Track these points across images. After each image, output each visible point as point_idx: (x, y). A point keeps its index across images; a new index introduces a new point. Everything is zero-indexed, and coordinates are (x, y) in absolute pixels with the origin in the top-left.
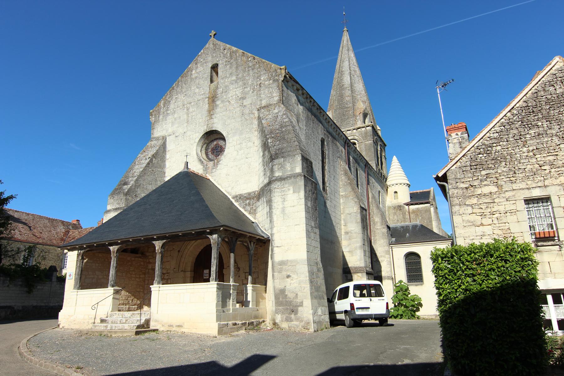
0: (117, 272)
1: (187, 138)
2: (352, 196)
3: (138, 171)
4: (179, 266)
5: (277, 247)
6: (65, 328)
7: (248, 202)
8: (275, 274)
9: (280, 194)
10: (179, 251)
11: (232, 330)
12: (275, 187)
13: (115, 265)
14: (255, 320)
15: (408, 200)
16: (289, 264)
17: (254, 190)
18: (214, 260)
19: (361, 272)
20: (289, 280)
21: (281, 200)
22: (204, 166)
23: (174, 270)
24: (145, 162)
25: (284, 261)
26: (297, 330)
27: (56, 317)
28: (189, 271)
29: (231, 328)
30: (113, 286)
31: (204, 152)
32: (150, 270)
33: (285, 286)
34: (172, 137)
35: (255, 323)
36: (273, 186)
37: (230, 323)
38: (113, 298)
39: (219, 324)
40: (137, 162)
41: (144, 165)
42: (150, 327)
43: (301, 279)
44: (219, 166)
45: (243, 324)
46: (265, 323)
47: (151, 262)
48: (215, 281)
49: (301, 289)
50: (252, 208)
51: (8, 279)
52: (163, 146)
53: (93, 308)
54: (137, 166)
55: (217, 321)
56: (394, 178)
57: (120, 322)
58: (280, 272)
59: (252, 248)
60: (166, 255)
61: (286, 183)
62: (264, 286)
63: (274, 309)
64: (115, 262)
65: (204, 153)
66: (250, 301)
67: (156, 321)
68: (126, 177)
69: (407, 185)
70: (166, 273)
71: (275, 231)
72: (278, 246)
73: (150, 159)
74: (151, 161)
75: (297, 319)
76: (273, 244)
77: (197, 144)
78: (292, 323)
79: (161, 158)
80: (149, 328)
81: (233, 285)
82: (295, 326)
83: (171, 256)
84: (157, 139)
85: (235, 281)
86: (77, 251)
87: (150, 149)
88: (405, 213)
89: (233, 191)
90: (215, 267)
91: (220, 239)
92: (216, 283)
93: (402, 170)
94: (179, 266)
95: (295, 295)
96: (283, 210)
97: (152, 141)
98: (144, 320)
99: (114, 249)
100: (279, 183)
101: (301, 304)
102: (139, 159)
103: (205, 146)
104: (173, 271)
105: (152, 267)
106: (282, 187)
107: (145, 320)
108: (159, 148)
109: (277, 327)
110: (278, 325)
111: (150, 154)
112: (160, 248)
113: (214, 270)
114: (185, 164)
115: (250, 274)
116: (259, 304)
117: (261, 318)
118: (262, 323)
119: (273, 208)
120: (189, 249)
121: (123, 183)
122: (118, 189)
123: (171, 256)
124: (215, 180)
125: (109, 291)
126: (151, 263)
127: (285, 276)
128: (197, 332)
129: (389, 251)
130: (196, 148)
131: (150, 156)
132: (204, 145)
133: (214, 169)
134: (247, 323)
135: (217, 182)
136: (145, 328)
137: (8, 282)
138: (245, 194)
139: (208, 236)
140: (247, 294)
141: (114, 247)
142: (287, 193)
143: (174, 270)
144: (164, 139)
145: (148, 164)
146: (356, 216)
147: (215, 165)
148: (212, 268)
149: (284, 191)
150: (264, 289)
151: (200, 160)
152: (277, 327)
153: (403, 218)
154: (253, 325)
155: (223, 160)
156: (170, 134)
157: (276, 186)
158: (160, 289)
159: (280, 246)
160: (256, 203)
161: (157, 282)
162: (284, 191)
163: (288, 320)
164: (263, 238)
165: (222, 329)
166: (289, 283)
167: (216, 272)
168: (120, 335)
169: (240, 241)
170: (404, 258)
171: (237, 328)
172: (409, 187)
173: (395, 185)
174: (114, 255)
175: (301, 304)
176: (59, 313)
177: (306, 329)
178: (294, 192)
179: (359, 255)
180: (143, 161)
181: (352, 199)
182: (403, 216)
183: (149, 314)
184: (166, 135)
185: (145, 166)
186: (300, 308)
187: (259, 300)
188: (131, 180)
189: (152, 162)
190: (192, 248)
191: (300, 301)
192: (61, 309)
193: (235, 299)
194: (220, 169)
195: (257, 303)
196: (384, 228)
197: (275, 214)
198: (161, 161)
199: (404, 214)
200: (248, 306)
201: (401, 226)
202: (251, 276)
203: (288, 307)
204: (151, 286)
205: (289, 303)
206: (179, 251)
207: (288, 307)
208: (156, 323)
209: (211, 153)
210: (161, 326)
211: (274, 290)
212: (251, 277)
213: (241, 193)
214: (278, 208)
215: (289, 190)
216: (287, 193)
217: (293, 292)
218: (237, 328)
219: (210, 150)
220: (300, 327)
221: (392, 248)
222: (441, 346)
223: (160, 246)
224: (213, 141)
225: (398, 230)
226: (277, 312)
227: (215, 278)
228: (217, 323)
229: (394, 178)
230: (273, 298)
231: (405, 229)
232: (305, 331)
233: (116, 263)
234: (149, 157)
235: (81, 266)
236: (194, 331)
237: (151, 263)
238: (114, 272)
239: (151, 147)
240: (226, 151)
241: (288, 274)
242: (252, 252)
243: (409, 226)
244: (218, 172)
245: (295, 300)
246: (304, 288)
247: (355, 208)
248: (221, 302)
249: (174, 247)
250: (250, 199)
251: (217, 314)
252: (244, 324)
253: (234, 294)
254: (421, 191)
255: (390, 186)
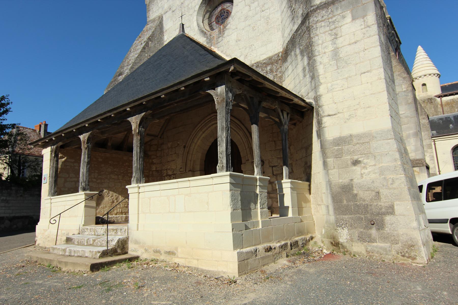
0: (90, 171)
1: (186, 9)
2: (399, 71)
3: (133, 58)
4: (186, 165)
5: (329, 116)
6: (40, 245)
7: (269, 68)
8: (328, 160)
9: (327, 29)
10: (184, 147)
11: (265, 261)
12: (317, 19)
13: (86, 160)
14: (300, 238)
15: (439, 92)
16: (355, 141)
17: (276, 52)
18: (222, 133)
19: (419, 165)
20: (357, 168)
21: (329, 38)
22: (207, 38)
23: (181, 170)
24: (140, 48)
25: (344, 137)
26: (388, 258)
27: (34, 230)
28: (199, 170)
29: (263, 258)
30: (84, 189)
31: (206, 22)
32: (154, 172)
33: (352, 180)
34: (169, 13)
35: (300, 243)
36: (313, 19)
37: (260, 247)
38: (86, 206)
39: (239, 254)
40: (132, 50)
41: (140, 50)
42: (129, 252)
43: (383, 164)
44: (226, 33)
45: (281, 247)
46: (314, 240)
47: (155, 162)
48: (227, 171)
49: (385, 184)
50: (277, 75)
51: (22, 188)
52: (159, 26)
53: (52, 221)
54: (132, 54)
55: (235, 247)
56: (424, 69)
57: (87, 242)
58: (338, 156)
59: (286, 122)
60: (170, 153)
61: (337, 9)
62: (308, 183)
63: (332, 218)
64: (86, 156)
65: (207, 24)
66: (288, 207)
67: (137, 242)
68: (121, 68)
69: (438, 75)
70: (172, 175)
71: (322, 90)
72: (331, 113)
73: (145, 43)
74: (147, 44)
75: (385, 238)
76: (321, 113)
77: (198, 13)
78: (375, 244)
79: (158, 40)
80: (126, 253)
81: (260, 178)
82: (382, 252)
83: (176, 153)
84: (154, 21)
85: (263, 173)
86: (50, 147)
87: (146, 33)
88: (437, 107)
89: (246, 60)
90: (224, 145)
91: (230, 95)
92: (228, 173)
93: (429, 60)
94: (186, 165)
95: (374, 193)
96: (336, 54)
97: (148, 24)
98: (116, 241)
99: (84, 137)
100: (323, 12)
101: (391, 210)
102: (134, 46)
103: (207, 16)
104: (180, 171)
105: (156, 169)
106: (330, 16)
107: (118, 242)
108: (155, 29)
109: (342, 250)
110: (343, 247)
111: (145, 38)
112: (138, 127)
113: (222, 151)
114: (180, 27)
115: (285, 164)
116: (302, 210)
117: (308, 233)
118: (309, 241)
119: (317, 54)
120: (196, 143)
121: (118, 74)
122: (113, 82)
123: (176, 153)
124: (222, 52)
125: (80, 196)
126: (155, 164)
127: (349, 162)
128: (200, 267)
129: (431, 145)
130: (197, 18)
131: (145, 39)
132: (206, 13)
133: (221, 38)
134: (289, 244)
135: (224, 54)
136: (119, 254)
137: (22, 192)
138: (263, 60)
139: (209, 91)
140: (282, 196)
141: (84, 135)
142: (340, 24)
143: (181, 170)
144: (161, 19)
145: (144, 48)
146: (407, 96)
147: (221, 33)
148: (219, 147)
149: (334, 22)
150: (308, 188)
151: (202, 32)
152: (342, 250)
153: (435, 111)
154: (298, 246)
155: (231, 23)
156: (167, 11)
157: (320, 18)
158: (141, 190)
159: (333, 113)
160: (281, 67)
161: (135, 179)
162: (334, 22)
163: (362, 238)
164: (303, 104)
165: (246, 261)
166: (359, 173)
167: (227, 155)
168: (71, 268)
169: (266, 110)
170: (451, 152)
171: (273, 256)
172: (439, 77)
173: (423, 76)
174: (84, 146)
175: (391, 210)
176: (37, 226)
177: (408, 257)
178: (354, 18)
179: (414, 144)
180: (139, 47)
181: (399, 75)
182: (435, 109)
183: (127, 230)
184: (163, 13)
185: (141, 52)
186: (388, 219)
187: (302, 205)
188: (126, 69)
189: (148, 46)
190: (199, 141)
191: (387, 204)
192: (38, 221)
193: (266, 204)
194: (228, 36)
195: (300, 210)
196: (424, 119)
197: (321, 63)
198: (158, 43)
199: (436, 107)
200: (287, 215)
201: (438, 118)
202: (287, 166)
203: (362, 216)
204: (127, 187)
205: (366, 208)
206: (184, 147)
207: (362, 216)
208: (136, 246)
209: (216, 23)
210: (143, 251)
211: (330, 187)
212: (287, 168)
213: (259, 60)
214: (325, 53)
215: (344, 17)
216: (340, 24)
217: (369, 189)
218: (273, 256)
219: (213, 19)
220: (394, 252)
221: (434, 142)
222: (37, 225)
223: (137, 123)
224: (217, 7)
225: (435, 122)
226: (339, 224)
227: (225, 165)
228: (236, 252)
229: (424, 69)
230: (327, 200)
231: (447, 121)
232: (405, 260)
233: (88, 158)
234: (145, 41)
235: (55, 165)
236: (194, 264)
237: (155, 164)
238: (85, 170)
239: (147, 31)
240: (233, 14)
241: (355, 157)
242: (286, 127)
243: (449, 118)
244: (225, 40)
245: (375, 204)
246: (393, 181)
247: (403, 86)
248: (240, 211)
249: (178, 143)
250: (272, 64)
251: (233, 235)
252: (283, 247)
253: (263, 196)
254: (450, 84)
255: (416, 79)
